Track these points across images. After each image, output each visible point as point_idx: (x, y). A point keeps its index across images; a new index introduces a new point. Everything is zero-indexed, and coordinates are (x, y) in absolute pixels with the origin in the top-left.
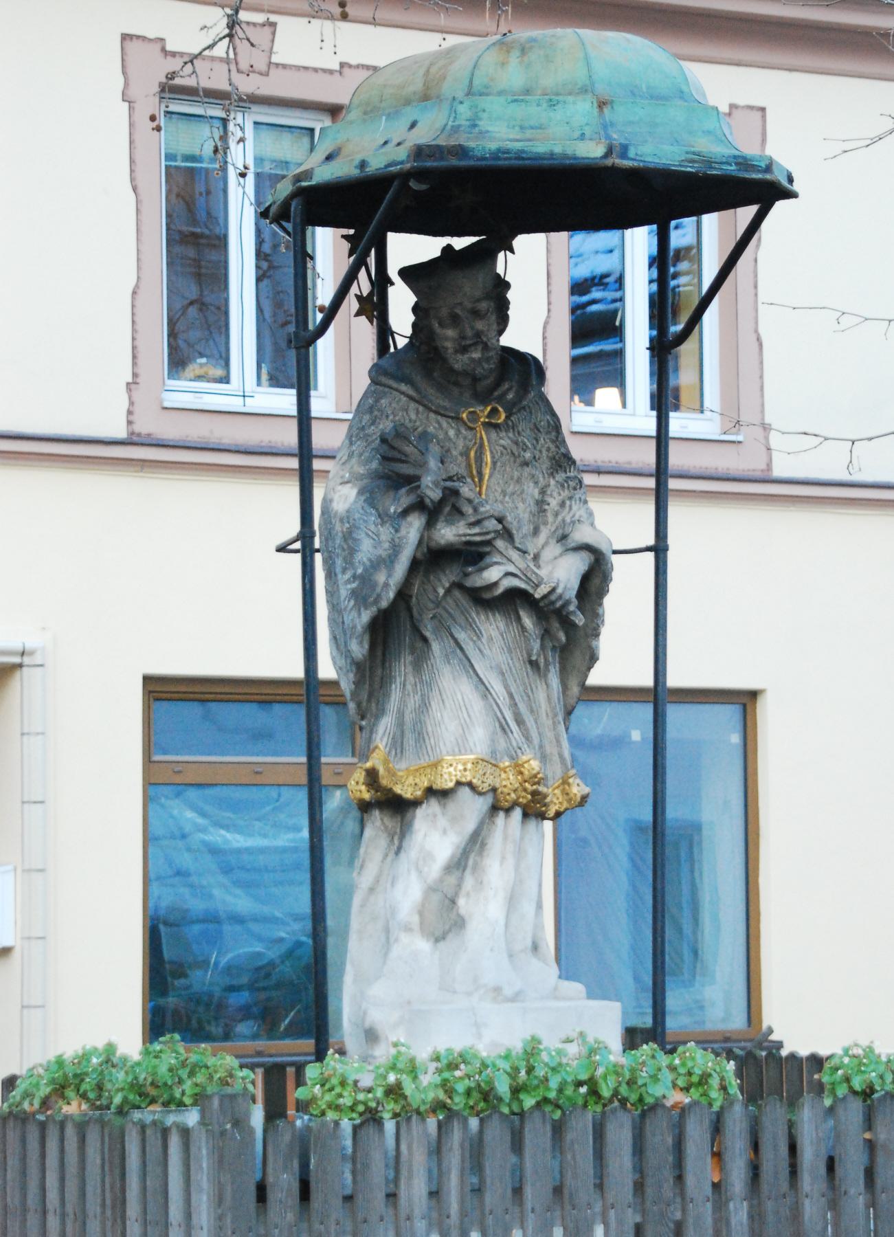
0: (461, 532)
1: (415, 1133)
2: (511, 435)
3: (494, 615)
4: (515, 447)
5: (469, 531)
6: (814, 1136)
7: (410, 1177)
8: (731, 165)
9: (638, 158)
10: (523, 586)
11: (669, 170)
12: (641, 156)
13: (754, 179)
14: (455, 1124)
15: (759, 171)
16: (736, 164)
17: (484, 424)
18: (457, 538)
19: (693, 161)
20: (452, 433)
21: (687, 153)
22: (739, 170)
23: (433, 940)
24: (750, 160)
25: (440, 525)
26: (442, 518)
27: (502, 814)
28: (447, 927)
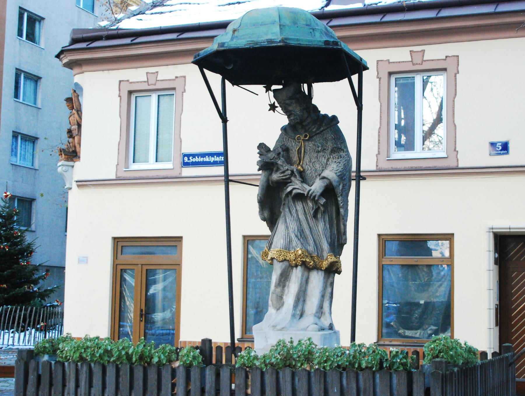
0: (278, 176)
1: (71, 367)
2: (313, 143)
3: (298, 203)
4: (314, 146)
5: (280, 176)
6: (210, 380)
7: (69, 382)
8: (265, 43)
9: (228, 46)
10: (302, 192)
11: (310, 47)
12: (230, 45)
13: (273, 46)
14: (84, 365)
15: (276, 43)
16: (267, 42)
17: (303, 140)
18: (278, 178)
19: (250, 44)
20: (293, 144)
21: (248, 41)
22: (269, 44)
23: (276, 310)
24: (273, 40)
25: (273, 174)
26: (274, 172)
27: (295, 268)
28: (280, 306)
